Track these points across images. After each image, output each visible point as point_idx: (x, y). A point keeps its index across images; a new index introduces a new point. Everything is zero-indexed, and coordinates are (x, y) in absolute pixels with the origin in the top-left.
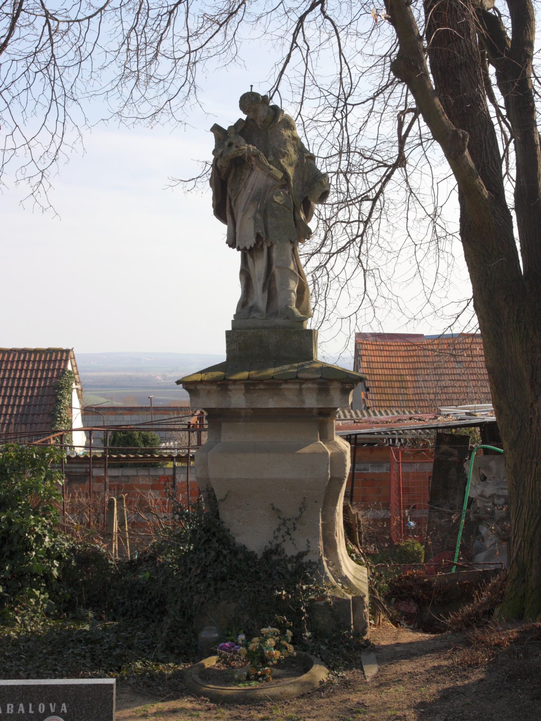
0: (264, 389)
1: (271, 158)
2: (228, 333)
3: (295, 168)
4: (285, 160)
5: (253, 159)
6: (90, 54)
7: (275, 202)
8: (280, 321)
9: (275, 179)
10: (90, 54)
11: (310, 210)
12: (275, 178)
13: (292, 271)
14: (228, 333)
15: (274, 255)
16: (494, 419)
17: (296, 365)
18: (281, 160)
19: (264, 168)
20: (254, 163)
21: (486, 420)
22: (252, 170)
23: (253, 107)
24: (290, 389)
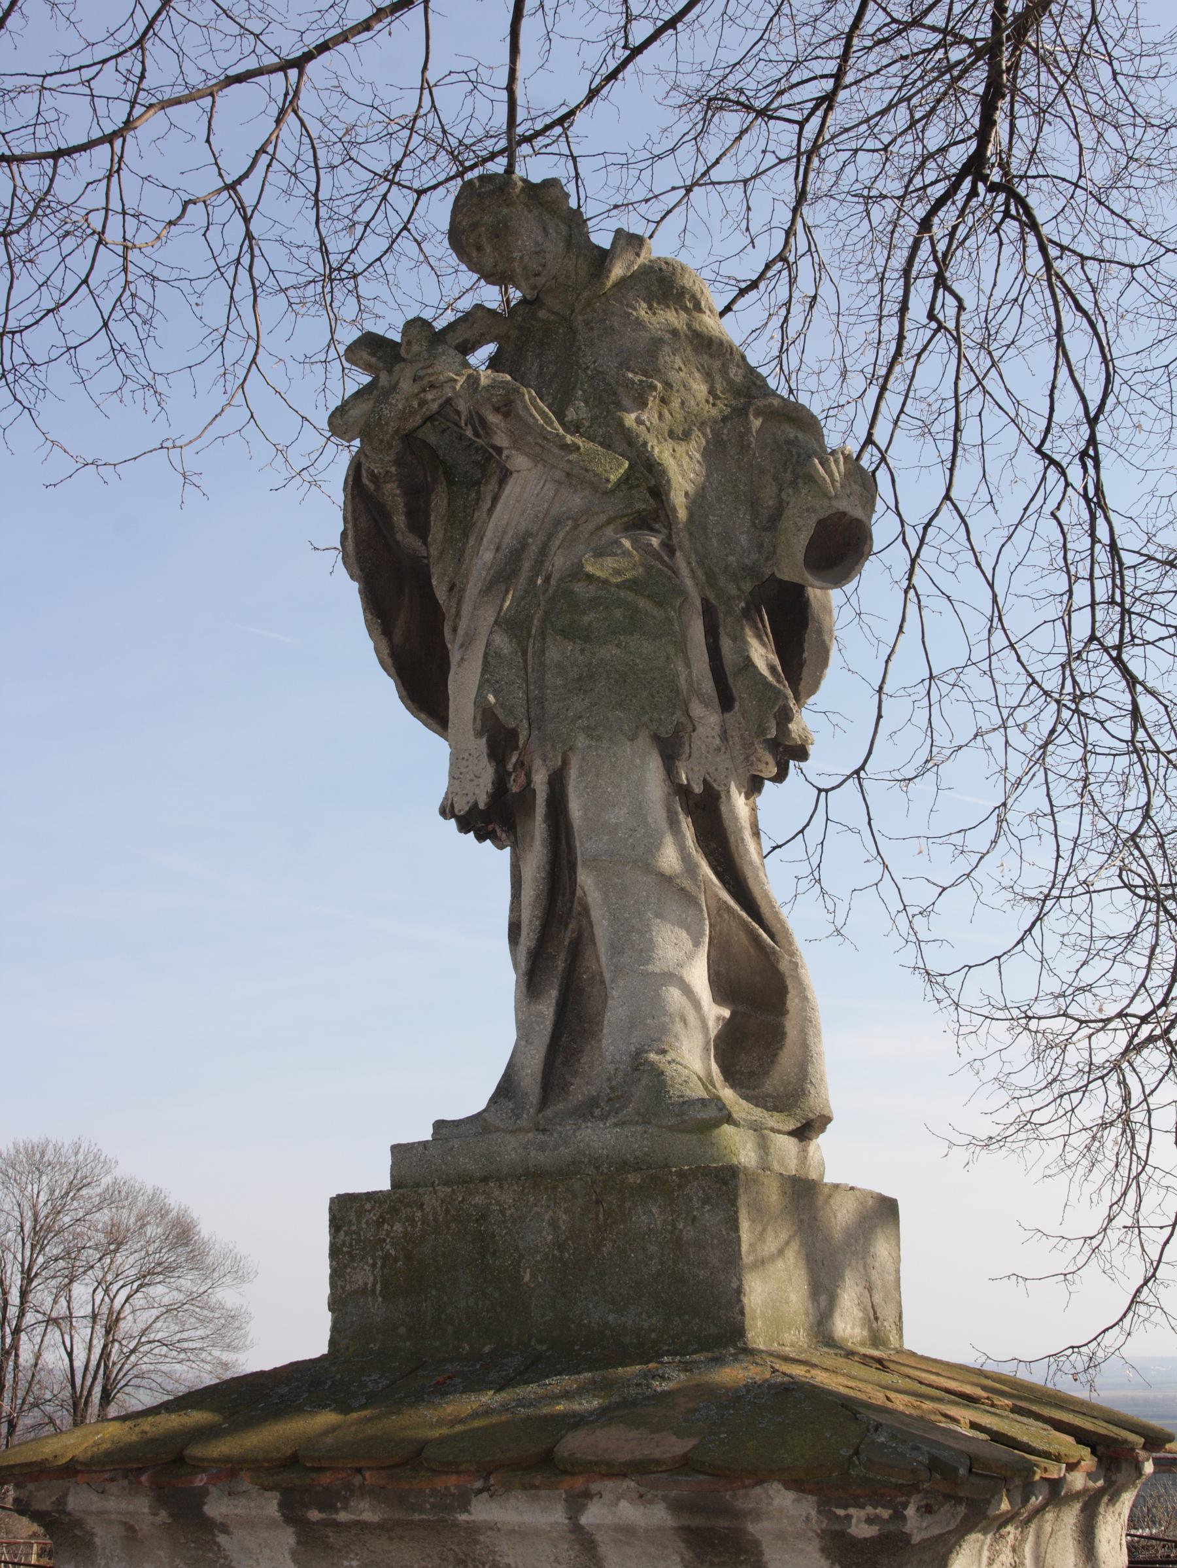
0: (382, 1528)
1: (578, 410)
2: (346, 1211)
3: (706, 453)
4: (649, 416)
5: (493, 419)
6: (85, 281)
7: (590, 577)
8: (599, 1138)
9: (595, 488)
10: (85, 281)
11: (810, 636)
12: (596, 486)
13: (666, 880)
14: (346, 1211)
15: (575, 808)
16: (397, 338)
17: (378, 1287)
18: (630, 419)
19: (543, 449)
20: (501, 440)
21: (821, 1378)
22: (505, 475)
23: (488, 219)
24: (520, 1534)
